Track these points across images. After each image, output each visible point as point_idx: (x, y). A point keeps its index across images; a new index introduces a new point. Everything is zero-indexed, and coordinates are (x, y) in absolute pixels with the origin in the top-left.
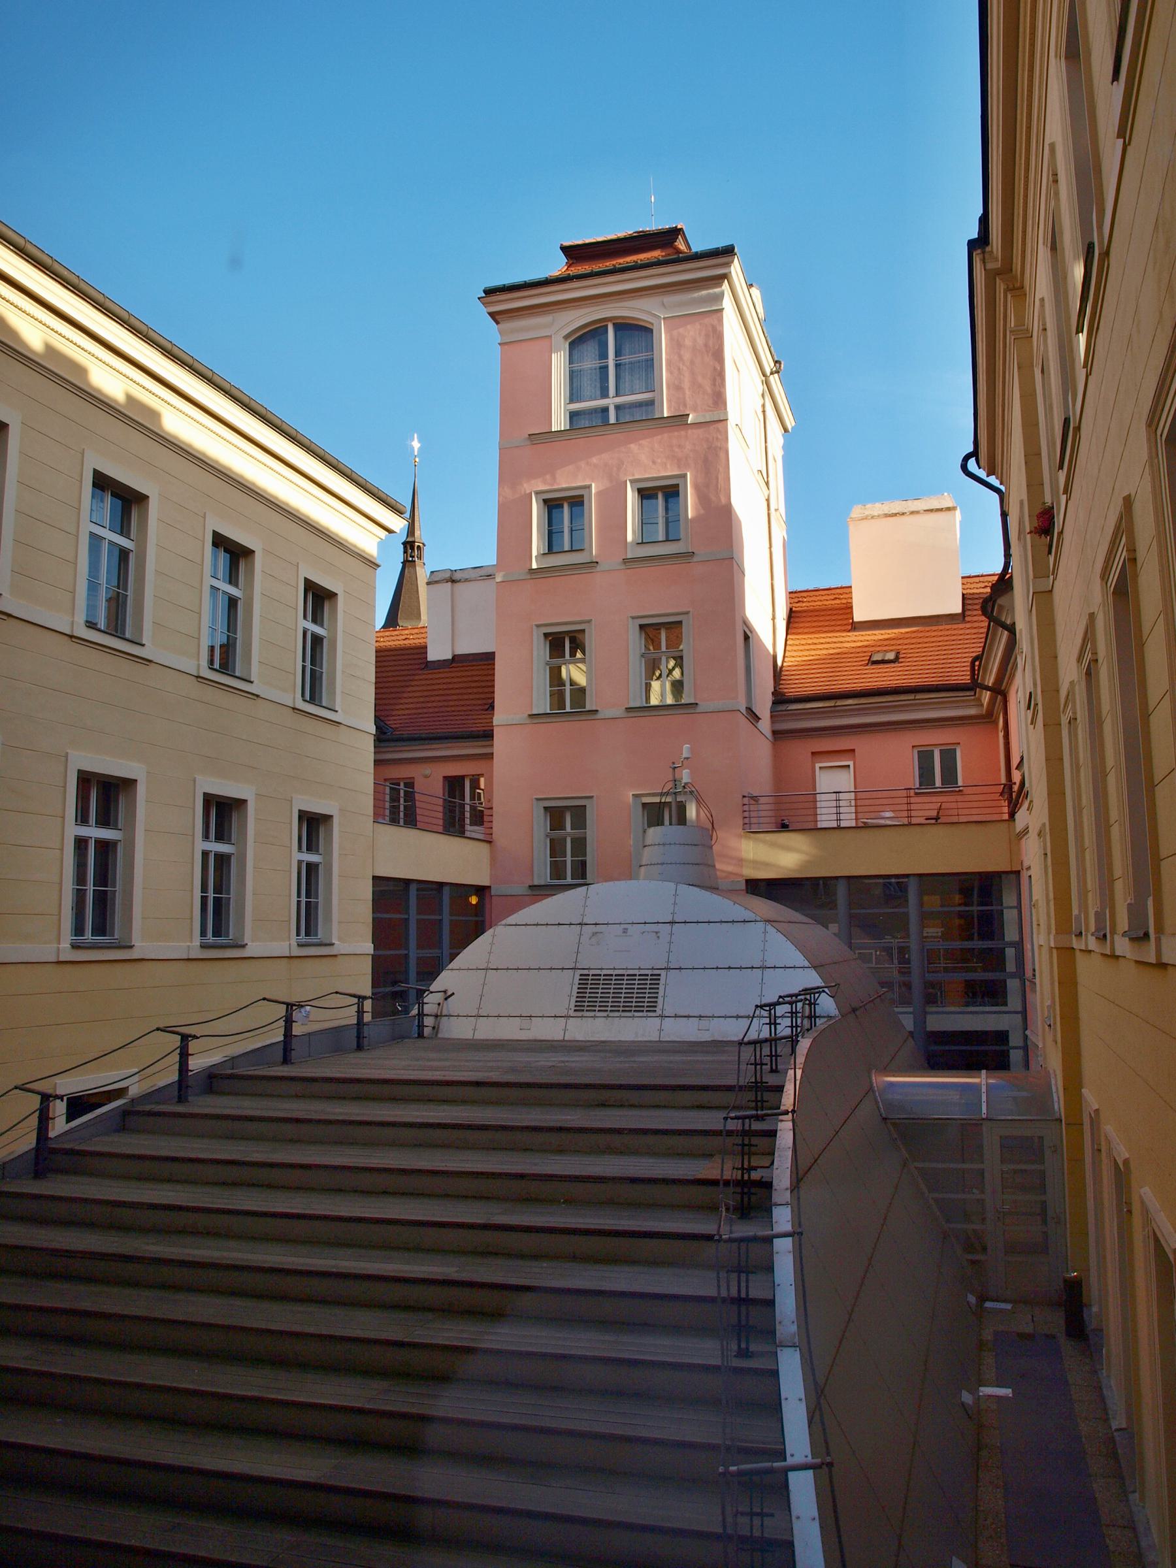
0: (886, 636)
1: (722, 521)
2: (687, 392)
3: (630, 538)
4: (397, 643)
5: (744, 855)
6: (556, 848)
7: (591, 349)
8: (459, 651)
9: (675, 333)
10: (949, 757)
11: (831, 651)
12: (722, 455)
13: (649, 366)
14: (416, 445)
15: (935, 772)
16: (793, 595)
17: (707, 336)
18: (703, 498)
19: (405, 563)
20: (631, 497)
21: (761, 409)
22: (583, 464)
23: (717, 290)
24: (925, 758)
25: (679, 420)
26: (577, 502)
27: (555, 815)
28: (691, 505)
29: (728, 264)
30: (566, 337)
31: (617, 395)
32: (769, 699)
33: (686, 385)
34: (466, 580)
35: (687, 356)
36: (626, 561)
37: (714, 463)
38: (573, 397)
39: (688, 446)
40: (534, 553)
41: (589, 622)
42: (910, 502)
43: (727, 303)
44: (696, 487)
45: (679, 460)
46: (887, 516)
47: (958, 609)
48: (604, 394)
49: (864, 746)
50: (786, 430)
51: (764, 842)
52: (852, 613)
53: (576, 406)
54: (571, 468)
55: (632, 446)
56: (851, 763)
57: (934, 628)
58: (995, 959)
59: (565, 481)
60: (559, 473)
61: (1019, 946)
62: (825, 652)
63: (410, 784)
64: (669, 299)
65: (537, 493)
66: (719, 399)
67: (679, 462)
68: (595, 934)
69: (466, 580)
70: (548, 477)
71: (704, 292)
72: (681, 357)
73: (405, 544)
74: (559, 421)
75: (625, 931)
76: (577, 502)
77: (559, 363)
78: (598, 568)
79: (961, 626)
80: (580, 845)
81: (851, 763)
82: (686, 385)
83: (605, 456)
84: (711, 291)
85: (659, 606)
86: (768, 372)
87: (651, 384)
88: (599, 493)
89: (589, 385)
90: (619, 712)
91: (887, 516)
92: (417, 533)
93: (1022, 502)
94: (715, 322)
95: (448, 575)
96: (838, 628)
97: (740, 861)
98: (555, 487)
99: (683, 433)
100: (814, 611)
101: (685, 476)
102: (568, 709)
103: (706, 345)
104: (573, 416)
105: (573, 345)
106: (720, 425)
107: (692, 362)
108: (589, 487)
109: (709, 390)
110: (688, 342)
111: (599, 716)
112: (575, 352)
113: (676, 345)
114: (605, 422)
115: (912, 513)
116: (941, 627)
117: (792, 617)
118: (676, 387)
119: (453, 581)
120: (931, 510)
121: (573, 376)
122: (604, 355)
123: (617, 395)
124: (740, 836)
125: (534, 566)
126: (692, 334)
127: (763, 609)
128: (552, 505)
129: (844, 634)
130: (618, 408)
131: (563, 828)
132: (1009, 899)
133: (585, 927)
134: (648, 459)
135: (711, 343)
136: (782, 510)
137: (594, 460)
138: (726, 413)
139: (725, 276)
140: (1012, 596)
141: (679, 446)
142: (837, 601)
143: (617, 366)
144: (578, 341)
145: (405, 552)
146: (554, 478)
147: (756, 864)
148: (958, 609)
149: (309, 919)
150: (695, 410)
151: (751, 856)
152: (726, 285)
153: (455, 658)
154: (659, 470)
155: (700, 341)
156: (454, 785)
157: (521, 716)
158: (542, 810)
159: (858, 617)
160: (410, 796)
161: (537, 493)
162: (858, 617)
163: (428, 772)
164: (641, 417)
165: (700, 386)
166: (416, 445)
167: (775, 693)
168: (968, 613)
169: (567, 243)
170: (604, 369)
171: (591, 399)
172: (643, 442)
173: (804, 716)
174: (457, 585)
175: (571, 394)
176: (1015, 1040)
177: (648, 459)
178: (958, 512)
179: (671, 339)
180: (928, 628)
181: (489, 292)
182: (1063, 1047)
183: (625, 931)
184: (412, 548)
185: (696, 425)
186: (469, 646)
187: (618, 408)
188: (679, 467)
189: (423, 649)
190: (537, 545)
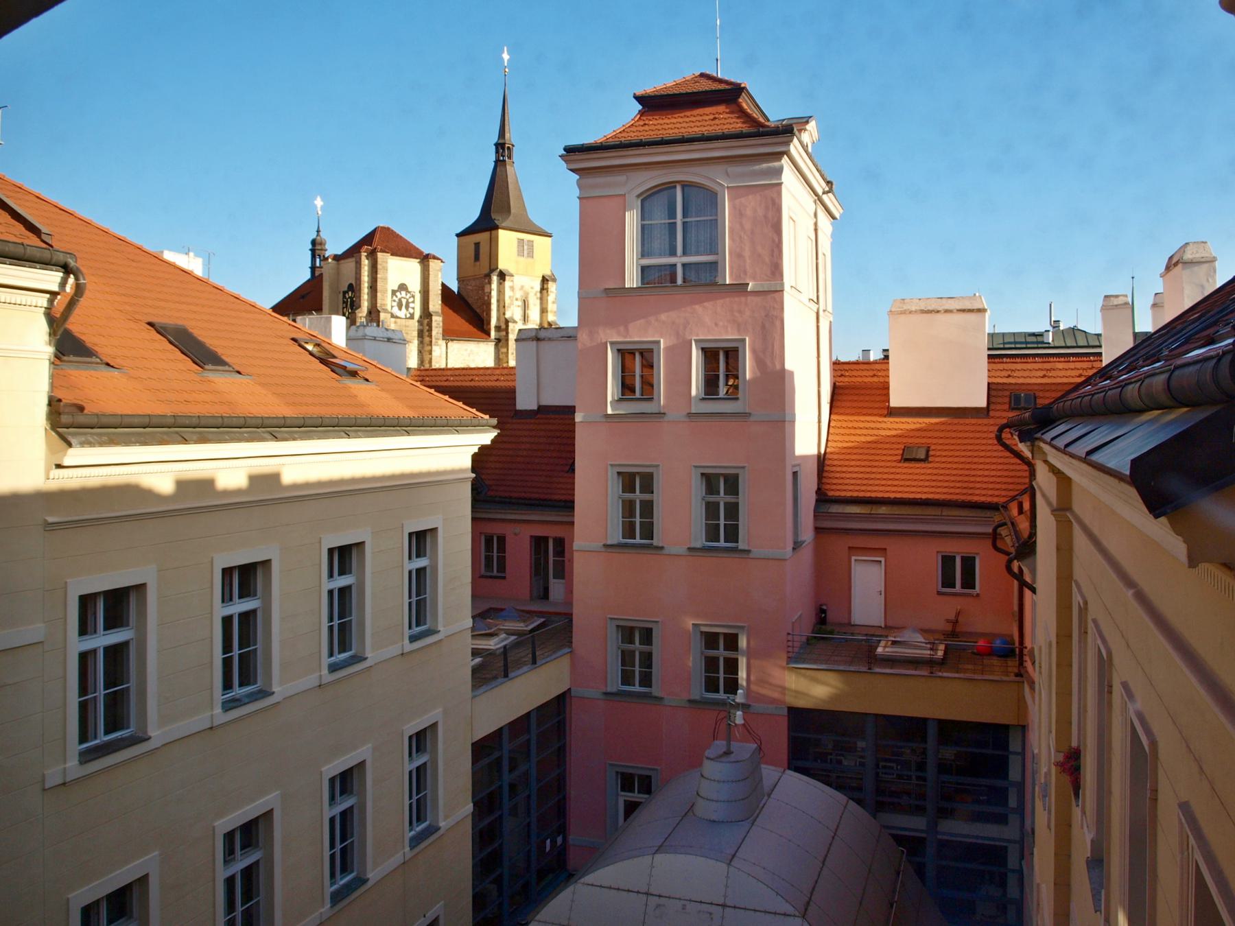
0: (918, 426)
1: (778, 384)
2: (748, 261)
3: (694, 392)
4: (489, 384)
5: (787, 685)
6: (626, 658)
7: (660, 202)
8: (545, 402)
9: (737, 202)
10: (968, 563)
11: (869, 439)
12: (778, 323)
13: (714, 225)
14: (506, 56)
15: (957, 574)
16: (836, 364)
17: (767, 208)
18: (759, 362)
19: (497, 162)
20: (695, 354)
21: (812, 228)
22: (652, 319)
23: (776, 164)
24: (948, 561)
25: (739, 288)
26: (647, 355)
27: (627, 633)
28: (749, 369)
29: (788, 143)
30: (638, 196)
31: (685, 253)
32: (812, 497)
33: (747, 253)
34: (550, 339)
35: (748, 226)
36: (690, 415)
37: (771, 327)
38: (644, 254)
39: (748, 313)
40: (609, 399)
41: (657, 466)
42: (944, 301)
43: (789, 177)
44: (754, 351)
45: (739, 325)
46: (923, 312)
47: (983, 403)
48: (673, 253)
49: (895, 547)
50: (834, 218)
51: (804, 676)
52: (888, 395)
53: (646, 262)
54: (642, 321)
55: (697, 307)
56: (883, 560)
57: (962, 421)
58: (1000, 795)
59: (638, 335)
60: (631, 326)
61: (1021, 786)
62: (863, 439)
63: (502, 540)
64: (733, 169)
65: (612, 343)
66: (776, 270)
67: (739, 327)
68: (658, 906)
69: (550, 339)
70: (622, 328)
71: (765, 166)
72: (741, 225)
73: (497, 145)
74: (632, 279)
75: (684, 907)
76: (647, 355)
77: (632, 220)
78: (666, 419)
79: (985, 421)
80: (647, 659)
81: (883, 560)
82: (747, 253)
83: (673, 315)
84: (771, 165)
85: (721, 461)
86: (820, 192)
87: (714, 245)
88: (667, 349)
89: (660, 241)
90: (682, 550)
91: (923, 312)
92: (507, 135)
93: (1050, 645)
94: (775, 196)
95: (534, 334)
96: (875, 411)
97: (783, 689)
98: (628, 340)
99: (743, 299)
100: (857, 387)
101: (744, 340)
102: (638, 395)
103: (765, 217)
104: (644, 270)
105: (643, 201)
106: (776, 295)
107: (752, 233)
108: (658, 342)
109: (767, 260)
110: (749, 212)
111: (665, 552)
112: (647, 204)
113: (738, 213)
114: (673, 280)
115: (946, 311)
116: (967, 421)
117: (837, 392)
118: (737, 255)
119: (538, 339)
120: (963, 311)
121: (644, 229)
122: (672, 214)
123: (685, 253)
124: (784, 668)
125: (610, 411)
126: (752, 204)
127: (809, 433)
128: (625, 354)
129: (881, 419)
130: (684, 265)
131: (632, 642)
132: (1014, 746)
133: (650, 898)
134: (711, 322)
135: (770, 215)
136: (830, 309)
137: (663, 317)
138: (782, 285)
139: (787, 153)
140: (1035, 561)
141: (740, 312)
142: (875, 379)
143: (684, 224)
144: (646, 198)
145: (497, 152)
146: (627, 329)
147: (797, 693)
148: (983, 403)
149: (420, 611)
150: (754, 279)
151: (793, 686)
152: (785, 161)
153: (543, 410)
154: (724, 334)
155: (760, 212)
156: (539, 543)
157: (597, 545)
158: (614, 628)
159: (895, 401)
160: (502, 548)
161: (612, 343)
162: (895, 401)
163: (517, 531)
164: (703, 280)
165: (759, 256)
166: (506, 56)
167: (819, 491)
168: (992, 407)
169: (639, 92)
170: (672, 226)
171: (660, 255)
172: (706, 304)
173: (842, 511)
174: (542, 344)
175: (643, 251)
176: (1012, 862)
177: (711, 322)
178: (987, 314)
179: (733, 207)
180: (956, 421)
181: (570, 150)
182: (1056, 836)
183: (684, 907)
184: (503, 149)
185: (754, 293)
186: (552, 398)
187: (684, 265)
188: (739, 331)
189: (511, 393)
190: (612, 389)
